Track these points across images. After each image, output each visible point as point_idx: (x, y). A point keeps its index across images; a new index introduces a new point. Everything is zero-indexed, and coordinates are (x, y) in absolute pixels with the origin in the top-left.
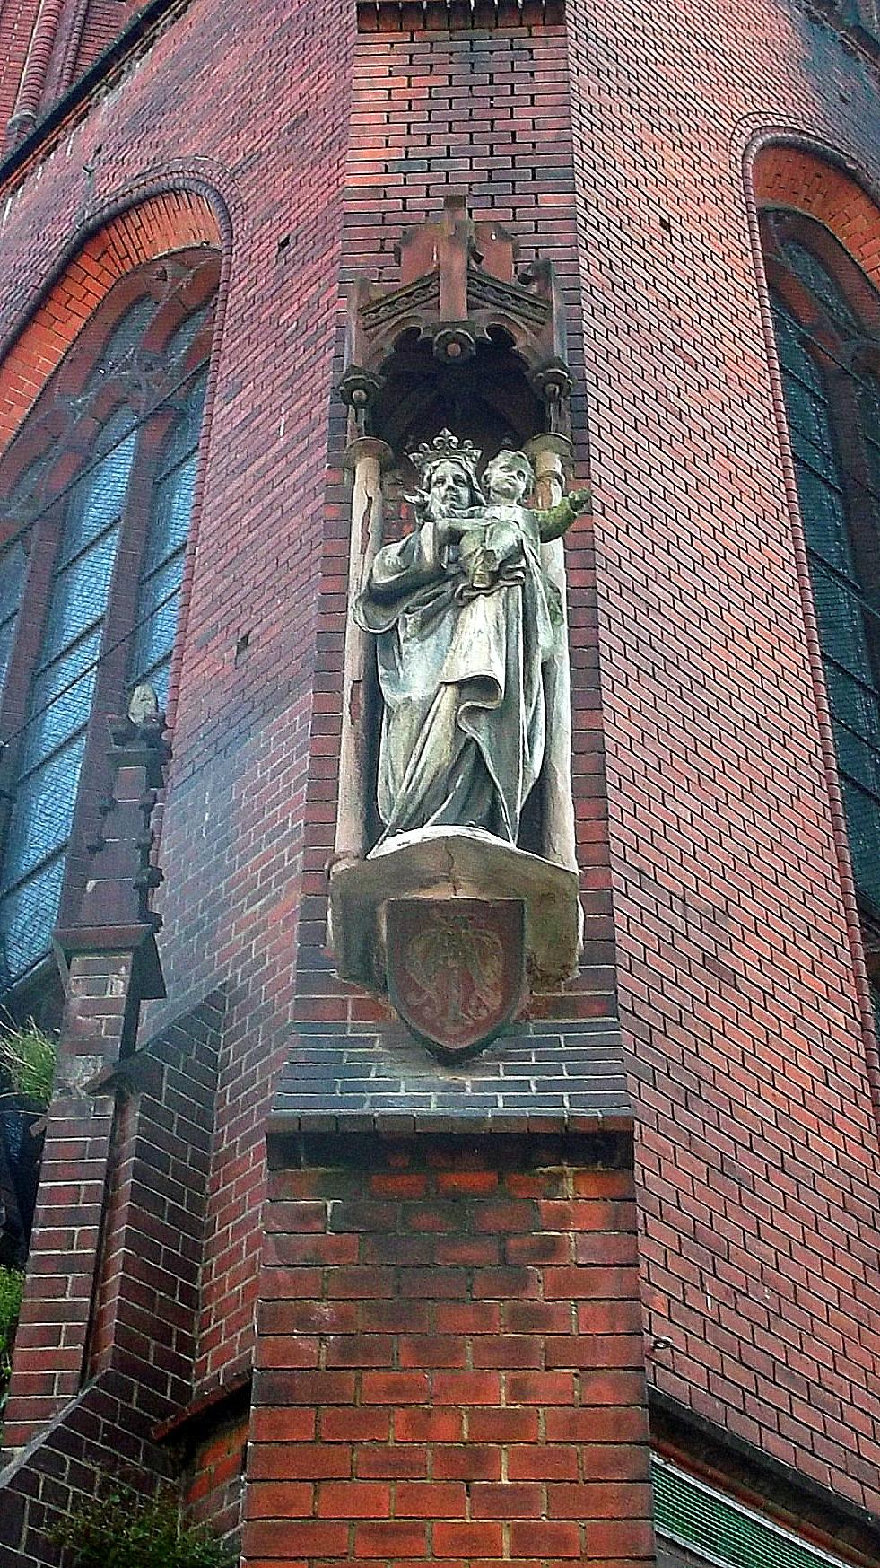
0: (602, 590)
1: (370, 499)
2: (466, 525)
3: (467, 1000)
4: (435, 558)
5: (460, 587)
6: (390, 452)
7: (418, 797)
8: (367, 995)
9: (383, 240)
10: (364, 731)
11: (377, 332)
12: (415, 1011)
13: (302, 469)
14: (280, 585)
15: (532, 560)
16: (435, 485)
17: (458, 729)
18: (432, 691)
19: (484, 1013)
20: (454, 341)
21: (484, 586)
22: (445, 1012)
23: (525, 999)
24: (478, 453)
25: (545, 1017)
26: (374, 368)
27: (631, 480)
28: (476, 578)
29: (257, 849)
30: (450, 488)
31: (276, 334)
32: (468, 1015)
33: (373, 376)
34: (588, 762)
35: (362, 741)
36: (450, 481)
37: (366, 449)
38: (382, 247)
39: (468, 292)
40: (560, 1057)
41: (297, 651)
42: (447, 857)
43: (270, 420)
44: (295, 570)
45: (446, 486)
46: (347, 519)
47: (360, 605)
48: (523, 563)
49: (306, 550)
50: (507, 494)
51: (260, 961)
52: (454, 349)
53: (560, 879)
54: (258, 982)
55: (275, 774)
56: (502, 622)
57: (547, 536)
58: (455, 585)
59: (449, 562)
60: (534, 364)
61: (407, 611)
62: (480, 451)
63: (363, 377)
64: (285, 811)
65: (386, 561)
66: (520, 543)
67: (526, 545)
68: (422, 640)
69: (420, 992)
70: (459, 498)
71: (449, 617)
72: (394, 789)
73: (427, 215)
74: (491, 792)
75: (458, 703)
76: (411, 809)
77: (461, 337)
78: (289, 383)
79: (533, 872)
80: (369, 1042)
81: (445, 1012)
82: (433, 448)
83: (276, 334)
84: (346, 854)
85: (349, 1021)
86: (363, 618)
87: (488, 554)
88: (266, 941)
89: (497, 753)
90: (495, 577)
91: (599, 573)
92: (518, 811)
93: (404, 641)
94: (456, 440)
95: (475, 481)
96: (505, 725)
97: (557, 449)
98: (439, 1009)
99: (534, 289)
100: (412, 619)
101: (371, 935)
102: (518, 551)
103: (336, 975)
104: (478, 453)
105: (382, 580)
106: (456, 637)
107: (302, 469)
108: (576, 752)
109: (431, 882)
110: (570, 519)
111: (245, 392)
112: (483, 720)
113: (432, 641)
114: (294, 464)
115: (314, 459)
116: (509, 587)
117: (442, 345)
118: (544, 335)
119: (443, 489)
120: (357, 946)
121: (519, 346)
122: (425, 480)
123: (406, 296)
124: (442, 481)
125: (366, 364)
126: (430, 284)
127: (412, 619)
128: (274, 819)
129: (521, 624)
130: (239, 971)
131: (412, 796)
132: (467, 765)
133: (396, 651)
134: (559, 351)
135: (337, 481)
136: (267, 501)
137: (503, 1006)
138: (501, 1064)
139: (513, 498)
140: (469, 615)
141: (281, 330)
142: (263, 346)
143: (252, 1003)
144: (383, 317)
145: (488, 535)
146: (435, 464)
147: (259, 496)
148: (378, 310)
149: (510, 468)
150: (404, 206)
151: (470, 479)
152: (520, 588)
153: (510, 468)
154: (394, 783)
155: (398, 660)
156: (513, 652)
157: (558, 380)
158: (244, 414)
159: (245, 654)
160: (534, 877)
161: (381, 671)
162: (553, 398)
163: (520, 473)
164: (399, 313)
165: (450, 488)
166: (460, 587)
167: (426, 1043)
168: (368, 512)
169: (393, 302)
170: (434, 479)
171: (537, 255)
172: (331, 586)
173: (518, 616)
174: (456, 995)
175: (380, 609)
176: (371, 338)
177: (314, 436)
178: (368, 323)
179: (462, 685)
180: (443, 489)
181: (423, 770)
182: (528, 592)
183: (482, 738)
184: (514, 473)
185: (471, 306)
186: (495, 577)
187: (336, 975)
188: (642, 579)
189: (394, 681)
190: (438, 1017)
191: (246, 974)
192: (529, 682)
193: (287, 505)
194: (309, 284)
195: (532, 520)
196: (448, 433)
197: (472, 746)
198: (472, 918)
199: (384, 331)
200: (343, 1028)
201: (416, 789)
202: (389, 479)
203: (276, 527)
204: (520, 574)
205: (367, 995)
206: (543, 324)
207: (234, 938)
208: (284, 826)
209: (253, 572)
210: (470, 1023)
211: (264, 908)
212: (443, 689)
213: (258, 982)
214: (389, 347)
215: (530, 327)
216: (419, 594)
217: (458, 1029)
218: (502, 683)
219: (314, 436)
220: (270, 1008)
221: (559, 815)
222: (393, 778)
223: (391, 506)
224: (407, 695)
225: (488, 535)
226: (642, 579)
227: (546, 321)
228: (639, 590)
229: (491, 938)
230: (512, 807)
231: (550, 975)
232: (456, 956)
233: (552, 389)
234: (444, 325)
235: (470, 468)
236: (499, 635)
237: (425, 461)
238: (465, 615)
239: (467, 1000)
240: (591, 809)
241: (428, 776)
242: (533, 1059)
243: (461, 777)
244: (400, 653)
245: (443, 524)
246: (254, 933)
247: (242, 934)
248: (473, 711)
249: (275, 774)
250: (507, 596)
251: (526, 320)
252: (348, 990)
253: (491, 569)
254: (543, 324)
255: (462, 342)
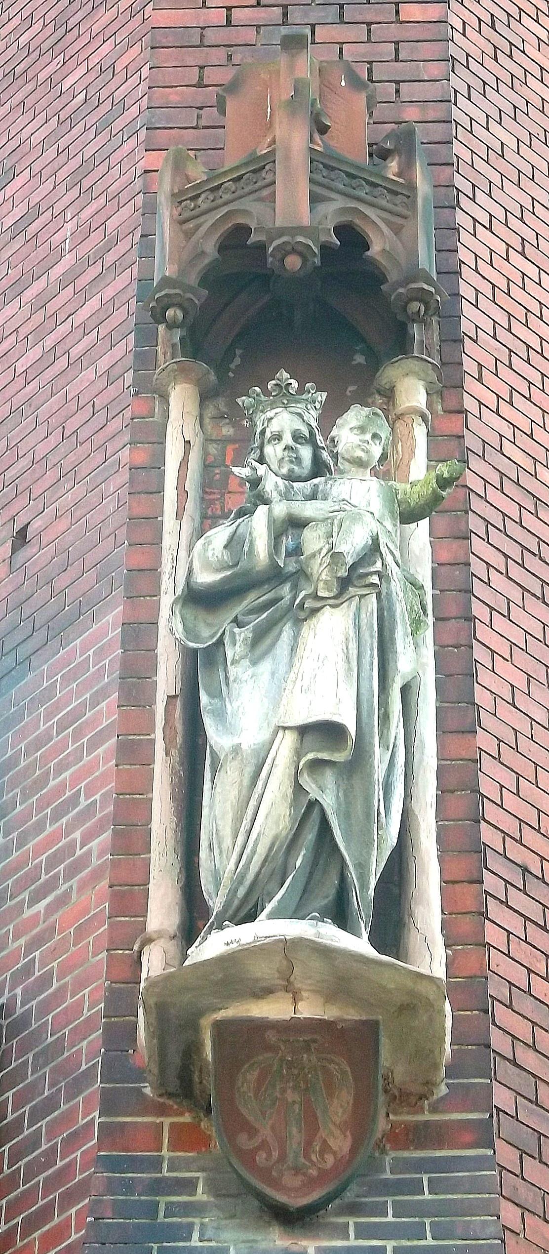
0: (478, 568)
1: (187, 443)
2: (309, 509)
3: (309, 1143)
4: (270, 556)
5: (302, 594)
6: (213, 377)
7: (250, 877)
8: (187, 1118)
9: (202, 68)
10: (182, 764)
11: (197, 227)
12: (248, 1158)
13: (94, 303)
14: (67, 464)
15: (389, 559)
16: (269, 442)
17: (298, 789)
18: (266, 735)
19: (330, 1160)
20: (294, 251)
21: (332, 595)
22: (282, 1158)
23: (382, 1125)
24: (322, 397)
25: (406, 1148)
26: (193, 279)
27: (517, 328)
28: (321, 585)
29: (40, 827)
30: (287, 448)
31: (57, 105)
32: (311, 1161)
33: (190, 289)
34: (459, 803)
35: (180, 777)
36: (288, 439)
37: (182, 372)
38: (201, 78)
39: (311, 181)
40: (422, 1210)
41: (91, 559)
42: (285, 963)
43: (52, 227)
44: (87, 445)
45: (282, 445)
46: (157, 465)
47: (177, 609)
48: (378, 566)
49: (101, 417)
50: (359, 463)
51: (45, 981)
52: (293, 262)
53: (423, 988)
54: (45, 1008)
55: (62, 727)
56: (353, 646)
57: (408, 516)
58: (295, 589)
59: (289, 554)
60: (393, 276)
61: (237, 622)
62: (325, 395)
63: (177, 291)
64: (76, 779)
65: (210, 554)
66: (376, 540)
67: (383, 540)
68: (254, 663)
69: (252, 1132)
70: (298, 460)
71: (287, 631)
72: (221, 863)
73: (258, 32)
74: (339, 867)
75: (299, 754)
76: (241, 892)
77: (300, 248)
78: (76, 179)
79: (389, 981)
80: (189, 1186)
81: (282, 1158)
82: (267, 393)
83: (57, 105)
84: (160, 934)
85: (165, 1152)
86: (180, 628)
87: (336, 557)
88: (54, 953)
89: (346, 815)
90: (344, 584)
91: (478, 545)
92: (373, 885)
93: (232, 664)
94: (295, 384)
95: (319, 438)
96: (357, 781)
97: (422, 375)
98: (275, 1154)
99: (393, 166)
100: (243, 634)
101: (192, 1050)
102: (374, 549)
103: (148, 1091)
104: (322, 397)
105: (205, 578)
106: (297, 663)
107: (94, 303)
108: (443, 791)
109: (263, 992)
110: (436, 499)
111: (18, 182)
112: (329, 777)
113: (266, 666)
114: (85, 294)
115: (109, 292)
116: (362, 596)
117: (279, 256)
118: (406, 233)
119: (280, 447)
120: (175, 1060)
121: (376, 249)
122: (257, 435)
123: (234, 180)
124: (278, 437)
125: (182, 272)
126: (263, 167)
127: (243, 634)
128: (60, 789)
129: (375, 645)
130: (19, 991)
131: (243, 876)
132: (310, 836)
133: (222, 677)
134: (426, 259)
135: (145, 413)
136: (49, 342)
137: (354, 1150)
138: (352, 1221)
139: (367, 468)
140: (312, 634)
141: (64, 99)
142: (41, 118)
143: (37, 1036)
144: (204, 206)
145: (335, 529)
146: (270, 414)
147: (40, 333)
148: (199, 195)
149: (362, 429)
150: (229, 17)
151: (311, 433)
152: (375, 595)
153: (362, 429)
154: (221, 853)
155: (224, 688)
156: (364, 684)
157: (423, 297)
158: (18, 213)
159: (23, 554)
160: (391, 986)
161: (204, 698)
162: (415, 317)
163: (375, 436)
164: (226, 203)
165: (287, 448)
166: (302, 594)
167: (260, 1196)
168: (185, 461)
169: (219, 187)
170: (268, 434)
171: (397, 91)
172: (140, 560)
173: (372, 637)
174: (296, 1136)
175: (202, 615)
176: (188, 235)
177: (110, 258)
178: (187, 214)
179: (303, 730)
180: (280, 447)
181: (254, 852)
182: (385, 603)
183: (329, 801)
184: (368, 437)
185: (315, 199)
186: (344, 584)
187: (148, 1091)
188: (528, 464)
189: (220, 715)
190: (275, 1163)
191: (28, 996)
192: (385, 718)
193: (76, 352)
194: (101, 38)
195: (391, 497)
196: (286, 375)
197: (316, 812)
198: (315, 1041)
199: (210, 223)
200: (156, 1164)
201: (247, 867)
202: (210, 411)
203: (61, 381)
204: (375, 579)
205: (187, 1118)
206: (405, 218)
207: (12, 946)
208: (74, 801)
209: (31, 440)
210: (313, 1172)
211: (51, 909)
212: (280, 734)
213: (45, 1008)
214: (210, 247)
215: (384, 220)
216: (251, 599)
217: (297, 1181)
218: (352, 729)
219: (110, 258)
220: (59, 1046)
221: (421, 880)
222: (220, 847)
223: (213, 449)
224: (236, 741)
225: (335, 529)
226: (528, 464)
227: (409, 213)
228: (525, 480)
229: (340, 1066)
230: (364, 886)
231: (411, 1094)
232: (295, 1088)
233: (415, 310)
234: (282, 232)
235: (312, 416)
236: (349, 662)
237: (258, 407)
238: (306, 630)
239: (309, 1143)
240: (461, 867)
241: (262, 851)
242: (390, 1212)
243: (302, 853)
244: (227, 678)
245: (280, 509)
246: (36, 943)
247: (22, 941)
248: (316, 765)
249: (62, 727)
250: (359, 609)
251: (385, 215)
252: (162, 1110)
253: (339, 574)
254: (405, 218)
255: (302, 252)
